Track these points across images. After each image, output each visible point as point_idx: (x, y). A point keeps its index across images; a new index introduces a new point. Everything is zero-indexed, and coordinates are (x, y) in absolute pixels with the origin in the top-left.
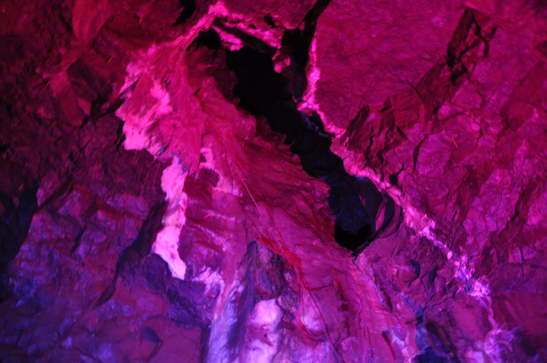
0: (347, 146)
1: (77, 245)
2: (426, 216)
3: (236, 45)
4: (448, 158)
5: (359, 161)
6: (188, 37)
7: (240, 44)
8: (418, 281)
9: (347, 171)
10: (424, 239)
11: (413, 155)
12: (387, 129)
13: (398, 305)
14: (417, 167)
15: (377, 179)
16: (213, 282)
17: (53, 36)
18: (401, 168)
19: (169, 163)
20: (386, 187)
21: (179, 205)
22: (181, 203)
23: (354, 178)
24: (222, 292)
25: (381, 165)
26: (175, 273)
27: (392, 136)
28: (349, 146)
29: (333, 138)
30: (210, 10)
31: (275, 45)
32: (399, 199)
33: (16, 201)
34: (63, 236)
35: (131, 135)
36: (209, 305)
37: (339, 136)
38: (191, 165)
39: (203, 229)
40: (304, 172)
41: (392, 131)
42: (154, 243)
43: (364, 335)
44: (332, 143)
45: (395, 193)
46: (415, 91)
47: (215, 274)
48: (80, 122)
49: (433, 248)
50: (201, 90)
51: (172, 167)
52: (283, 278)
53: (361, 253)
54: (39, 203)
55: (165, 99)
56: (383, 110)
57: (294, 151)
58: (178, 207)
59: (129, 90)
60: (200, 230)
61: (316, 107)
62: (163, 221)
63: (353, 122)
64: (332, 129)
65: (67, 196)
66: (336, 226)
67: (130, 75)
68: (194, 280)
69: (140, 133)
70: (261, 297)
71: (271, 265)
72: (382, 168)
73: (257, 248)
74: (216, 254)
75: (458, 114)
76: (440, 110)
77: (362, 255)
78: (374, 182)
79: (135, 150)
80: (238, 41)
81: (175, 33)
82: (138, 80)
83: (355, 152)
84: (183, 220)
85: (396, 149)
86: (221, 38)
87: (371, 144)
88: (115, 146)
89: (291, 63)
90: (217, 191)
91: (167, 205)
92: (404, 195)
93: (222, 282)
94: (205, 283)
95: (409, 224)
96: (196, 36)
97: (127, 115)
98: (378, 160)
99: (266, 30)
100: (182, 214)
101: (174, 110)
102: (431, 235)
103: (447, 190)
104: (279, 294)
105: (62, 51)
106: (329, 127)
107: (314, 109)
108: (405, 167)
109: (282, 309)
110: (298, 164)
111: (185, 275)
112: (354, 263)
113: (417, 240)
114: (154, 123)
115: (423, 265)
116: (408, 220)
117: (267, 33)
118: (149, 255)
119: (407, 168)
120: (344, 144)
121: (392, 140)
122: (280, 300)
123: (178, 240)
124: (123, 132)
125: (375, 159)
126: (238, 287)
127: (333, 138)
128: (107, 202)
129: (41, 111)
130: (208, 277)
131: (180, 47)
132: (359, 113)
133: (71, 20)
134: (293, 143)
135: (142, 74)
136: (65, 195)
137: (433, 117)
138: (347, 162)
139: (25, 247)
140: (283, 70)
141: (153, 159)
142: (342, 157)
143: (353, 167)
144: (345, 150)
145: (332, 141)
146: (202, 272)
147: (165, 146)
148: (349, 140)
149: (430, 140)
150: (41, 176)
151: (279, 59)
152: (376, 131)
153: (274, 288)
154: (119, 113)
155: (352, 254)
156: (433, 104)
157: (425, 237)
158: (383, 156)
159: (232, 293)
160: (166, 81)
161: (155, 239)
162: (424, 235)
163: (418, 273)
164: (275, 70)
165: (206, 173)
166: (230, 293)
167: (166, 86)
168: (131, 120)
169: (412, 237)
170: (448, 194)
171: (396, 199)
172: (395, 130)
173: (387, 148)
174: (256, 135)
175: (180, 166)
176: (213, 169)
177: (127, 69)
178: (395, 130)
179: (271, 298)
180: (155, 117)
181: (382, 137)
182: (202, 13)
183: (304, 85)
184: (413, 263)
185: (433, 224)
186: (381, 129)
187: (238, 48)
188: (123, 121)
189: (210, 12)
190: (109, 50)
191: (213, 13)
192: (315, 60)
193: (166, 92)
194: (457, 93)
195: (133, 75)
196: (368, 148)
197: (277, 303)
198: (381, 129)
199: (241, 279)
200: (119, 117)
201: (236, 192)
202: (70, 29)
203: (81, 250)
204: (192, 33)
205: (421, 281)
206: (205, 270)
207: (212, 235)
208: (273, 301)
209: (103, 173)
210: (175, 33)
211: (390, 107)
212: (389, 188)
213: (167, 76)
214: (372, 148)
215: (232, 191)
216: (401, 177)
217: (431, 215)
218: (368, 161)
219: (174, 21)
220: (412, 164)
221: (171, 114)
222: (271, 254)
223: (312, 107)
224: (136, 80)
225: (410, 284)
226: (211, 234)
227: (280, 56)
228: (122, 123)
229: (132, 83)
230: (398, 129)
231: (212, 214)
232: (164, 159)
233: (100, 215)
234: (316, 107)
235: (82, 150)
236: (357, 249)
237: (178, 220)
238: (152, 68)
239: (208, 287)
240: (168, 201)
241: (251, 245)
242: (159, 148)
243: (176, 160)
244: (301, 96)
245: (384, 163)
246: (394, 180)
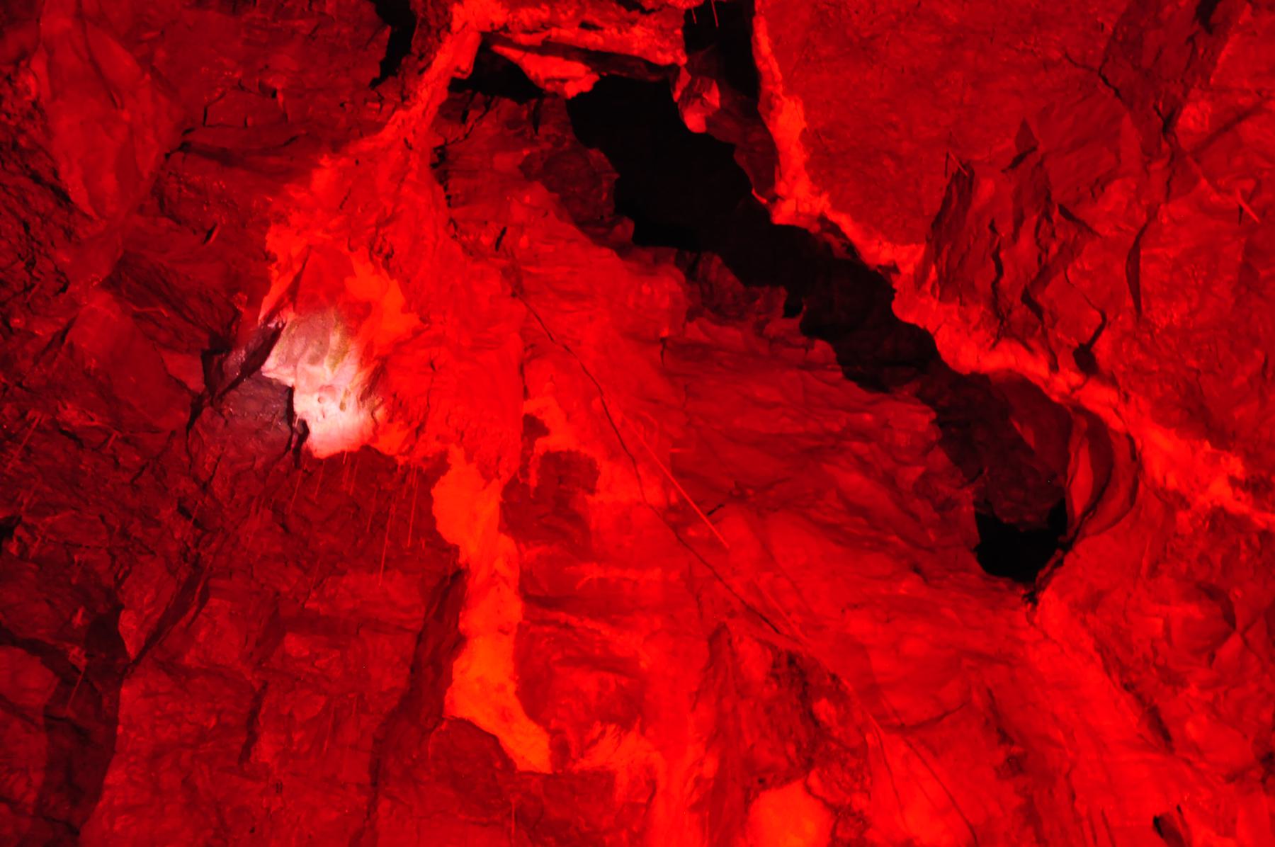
0: (938, 293)
1: (253, 738)
2: (1207, 446)
3: (575, 79)
4: (1240, 259)
5: (976, 328)
6: (419, 108)
7: (587, 72)
8: (1234, 643)
9: (950, 364)
10: (1219, 519)
11: (1125, 278)
12: (1035, 218)
13: (1190, 727)
14: (1143, 307)
15: (1037, 369)
16: (632, 762)
17: (26, 226)
18: (1100, 321)
19: (440, 466)
20: (1069, 385)
21: (496, 572)
22: (500, 565)
23: (979, 380)
24: (662, 785)
25: (1040, 327)
26: (523, 758)
27: (1053, 235)
28: (942, 292)
29: (894, 276)
30: (455, 17)
31: (669, 59)
32: (1116, 411)
33: (75, 653)
34: (213, 722)
35: (320, 418)
36: (635, 828)
37: (909, 269)
38: (499, 459)
39: (574, 620)
40: (852, 385)
41: (1050, 220)
42: (449, 694)
43: (1095, 838)
44: (895, 291)
45: (1099, 398)
46: (1101, 81)
47: (631, 740)
48: (184, 417)
49: (1255, 540)
50: (509, 231)
51: (451, 474)
52: (811, 717)
53: (1044, 589)
54: (131, 650)
55: (393, 298)
56: (1018, 160)
57: (812, 330)
58: (494, 575)
59: (286, 301)
60: (567, 626)
61: (822, 204)
62: (462, 625)
63: (938, 219)
64: (879, 252)
65: (197, 612)
66: (980, 518)
67: (281, 258)
68: (577, 767)
69: (342, 407)
70: (761, 781)
71: (775, 686)
72: (1045, 333)
73: (730, 642)
74: (624, 682)
75: (1242, 115)
76: (1180, 121)
77: (1047, 596)
78: (1033, 380)
79: (343, 452)
80: (578, 68)
81: (382, 106)
82: (304, 265)
83: (962, 303)
84: (515, 610)
85: (1069, 272)
86: (529, 72)
87: (1000, 270)
88: (290, 454)
89: (721, 99)
90: (601, 503)
91: (466, 578)
92: (1127, 398)
93: (656, 757)
94: (611, 767)
95: (1165, 479)
96: (443, 96)
97: (295, 367)
98: (1029, 313)
99: (633, 23)
100: (509, 594)
101: (423, 320)
102: (1239, 499)
103: (1259, 354)
104: (809, 764)
105: (64, 258)
106: (875, 248)
107: (818, 211)
108: (1109, 317)
109: (827, 805)
110: (829, 367)
111: (551, 758)
112: (1032, 623)
113: (1200, 522)
114: (376, 369)
115: (1238, 592)
116: (1156, 467)
117: (638, 31)
118: (444, 726)
119: (1116, 317)
120: (928, 289)
121: (1054, 248)
122: (814, 781)
123: (510, 668)
124: (296, 416)
125: (1020, 312)
126: (700, 763)
127: (894, 276)
128: (306, 606)
129: (71, 414)
130: (615, 750)
131: (406, 141)
132: (949, 188)
133: (55, 174)
134: (805, 308)
135: (309, 247)
136: (191, 613)
137: (1165, 146)
138: (943, 340)
139: (115, 777)
140: (709, 122)
141: (396, 466)
142: (931, 329)
143: (964, 349)
144: (934, 305)
145: (895, 286)
146: (595, 742)
147: (416, 424)
148: (939, 272)
149: (1165, 220)
150: (120, 575)
151: (692, 95)
152: (1005, 230)
153: (791, 749)
154: (273, 367)
155: (1025, 596)
156: (1156, 108)
157: (1222, 509)
158: (1039, 299)
159: (690, 784)
160: (380, 251)
161: (450, 681)
162: (1217, 503)
163: (1230, 619)
164: (689, 127)
165: (558, 463)
166: (685, 783)
167: (386, 261)
168: (310, 377)
169: (1183, 517)
170: (1265, 366)
171: (1106, 414)
172: (1056, 215)
173: (1044, 273)
174: (692, 315)
175: (473, 467)
176: (573, 447)
177: (268, 245)
178: (1056, 215)
179: (788, 780)
180: (376, 352)
181: (1026, 242)
182: (438, 31)
183: (769, 153)
184: (1211, 593)
185: (1236, 466)
186: (1019, 222)
187: (587, 87)
188: (290, 385)
189: (457, 24)
190: (205, 209)
191: (466, 24)
192: (779, 76)
193: (392, 278)
194: (1223, 55)
195: (290, 257)
196: (995, 286)
197: (808, 790)
198: (1019, 222)
199: (705, 739)
200: (275, 379)
201: (653, 495)
202: (62, 197)
203: (266, 750)
204: (425, 94)
205: (1246, 642)
206: (603, 734)
207: (603, 632)
208: (796, 789)
209: (280, 530)
210: (382, 106)
211: (1035, 149)
212: (1080, 387)
213: (381, 232)
214: (1005, 281)
215: (643, 494)
216: (1103, 349)
217: (1222, 437)
218: (1002, 323)
219: (376, 73)
220: (1129, 303)
221: (416, 332)
222: (769, 653)
223: (811, 205)
224: (297, 268)
225: (1213, 656)
226: (599, 632)
227: (692, 83)
228: (290, 391)
229: (289, 279)
230: (1064, 211)
231: (593, 572)
232: (426, 459)
233: (294, 644)
234: (822, 204)
235: (205, 487)
236: (1037, 579)
237: (499, 612)
238: (334, 223)
239: (623, 779)
240: (468, 565)
241: (717, 636)
242: (403, 434)
243: (457, 453)
244: (771, 182)
245: (1047, 317)
246: (1085, 360)
